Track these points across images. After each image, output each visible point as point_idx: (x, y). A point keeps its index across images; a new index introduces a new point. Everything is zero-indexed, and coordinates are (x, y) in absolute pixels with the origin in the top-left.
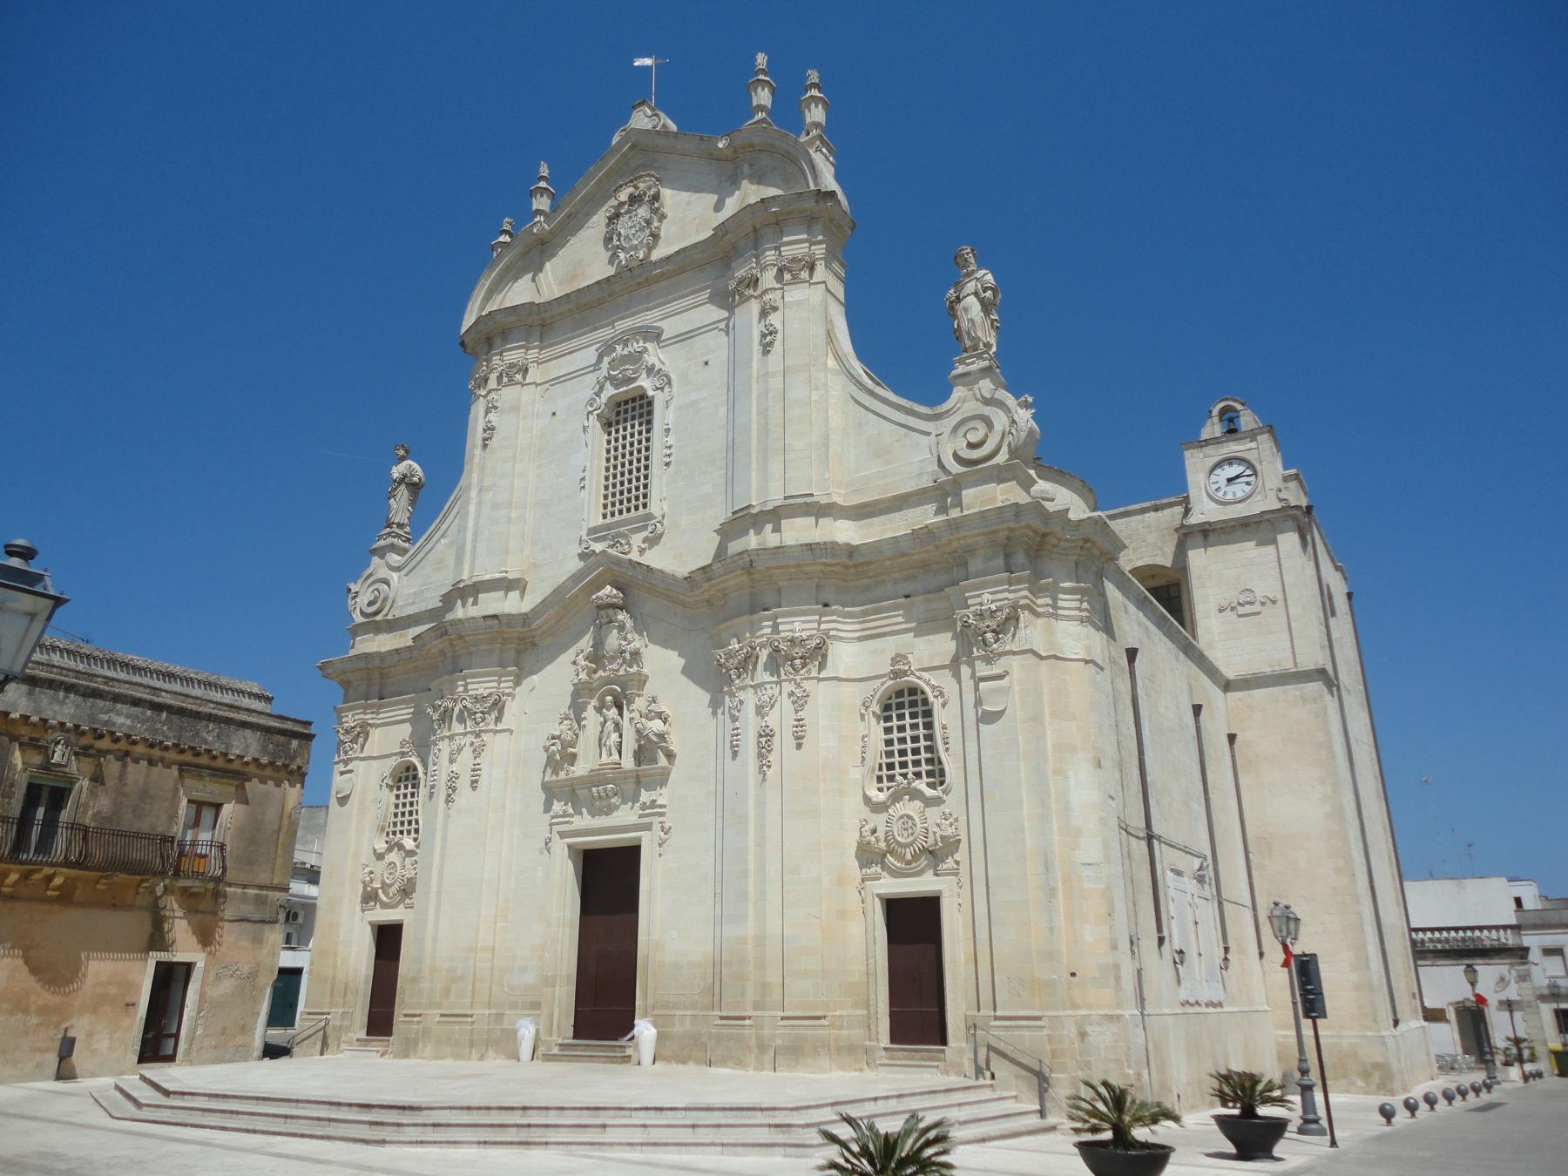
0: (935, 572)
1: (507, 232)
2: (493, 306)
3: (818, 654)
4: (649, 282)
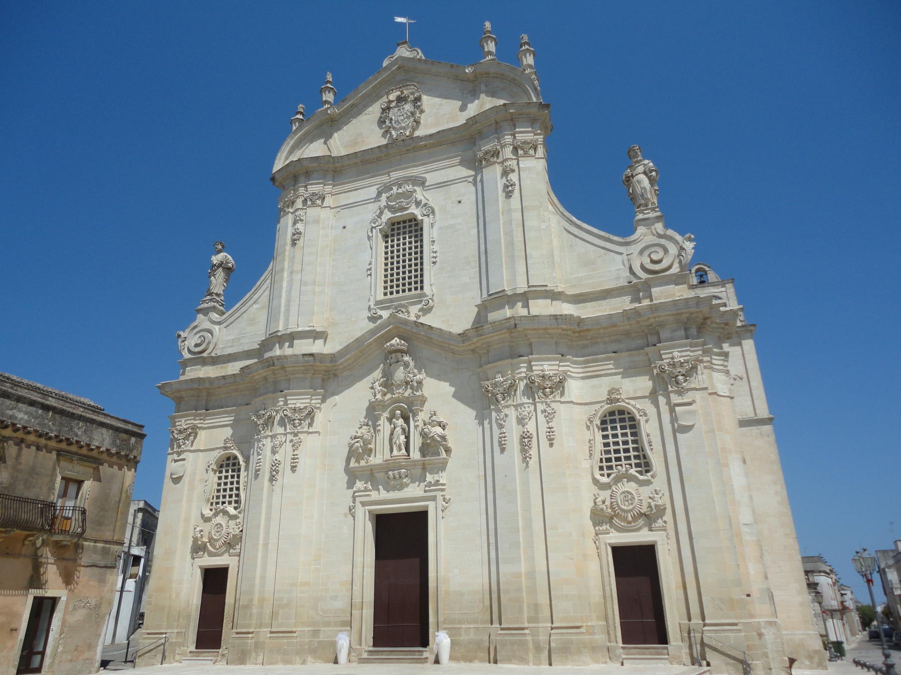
0: (636, 338)
1: (301, 113)
2: (294, 158)
3: (559, 385)
4: (415, 149)
